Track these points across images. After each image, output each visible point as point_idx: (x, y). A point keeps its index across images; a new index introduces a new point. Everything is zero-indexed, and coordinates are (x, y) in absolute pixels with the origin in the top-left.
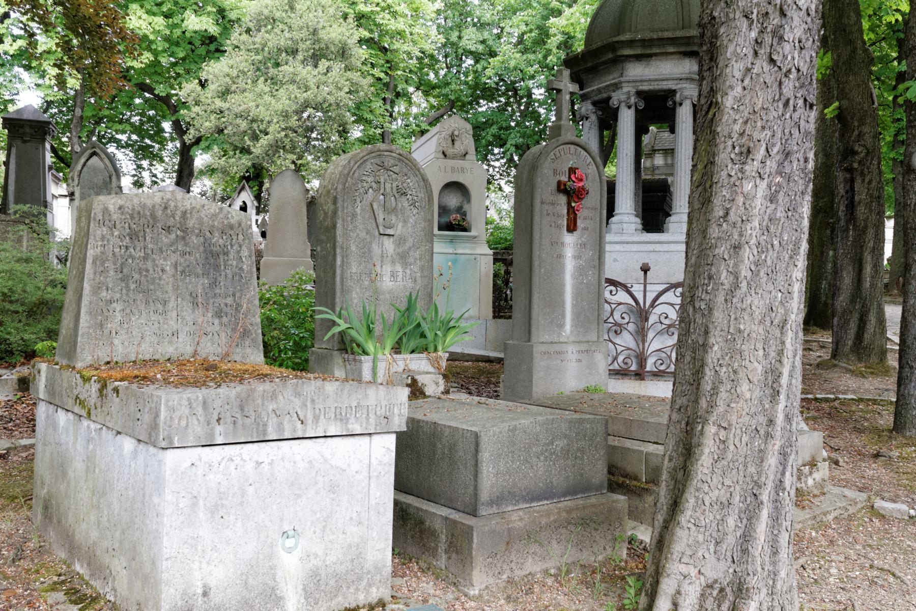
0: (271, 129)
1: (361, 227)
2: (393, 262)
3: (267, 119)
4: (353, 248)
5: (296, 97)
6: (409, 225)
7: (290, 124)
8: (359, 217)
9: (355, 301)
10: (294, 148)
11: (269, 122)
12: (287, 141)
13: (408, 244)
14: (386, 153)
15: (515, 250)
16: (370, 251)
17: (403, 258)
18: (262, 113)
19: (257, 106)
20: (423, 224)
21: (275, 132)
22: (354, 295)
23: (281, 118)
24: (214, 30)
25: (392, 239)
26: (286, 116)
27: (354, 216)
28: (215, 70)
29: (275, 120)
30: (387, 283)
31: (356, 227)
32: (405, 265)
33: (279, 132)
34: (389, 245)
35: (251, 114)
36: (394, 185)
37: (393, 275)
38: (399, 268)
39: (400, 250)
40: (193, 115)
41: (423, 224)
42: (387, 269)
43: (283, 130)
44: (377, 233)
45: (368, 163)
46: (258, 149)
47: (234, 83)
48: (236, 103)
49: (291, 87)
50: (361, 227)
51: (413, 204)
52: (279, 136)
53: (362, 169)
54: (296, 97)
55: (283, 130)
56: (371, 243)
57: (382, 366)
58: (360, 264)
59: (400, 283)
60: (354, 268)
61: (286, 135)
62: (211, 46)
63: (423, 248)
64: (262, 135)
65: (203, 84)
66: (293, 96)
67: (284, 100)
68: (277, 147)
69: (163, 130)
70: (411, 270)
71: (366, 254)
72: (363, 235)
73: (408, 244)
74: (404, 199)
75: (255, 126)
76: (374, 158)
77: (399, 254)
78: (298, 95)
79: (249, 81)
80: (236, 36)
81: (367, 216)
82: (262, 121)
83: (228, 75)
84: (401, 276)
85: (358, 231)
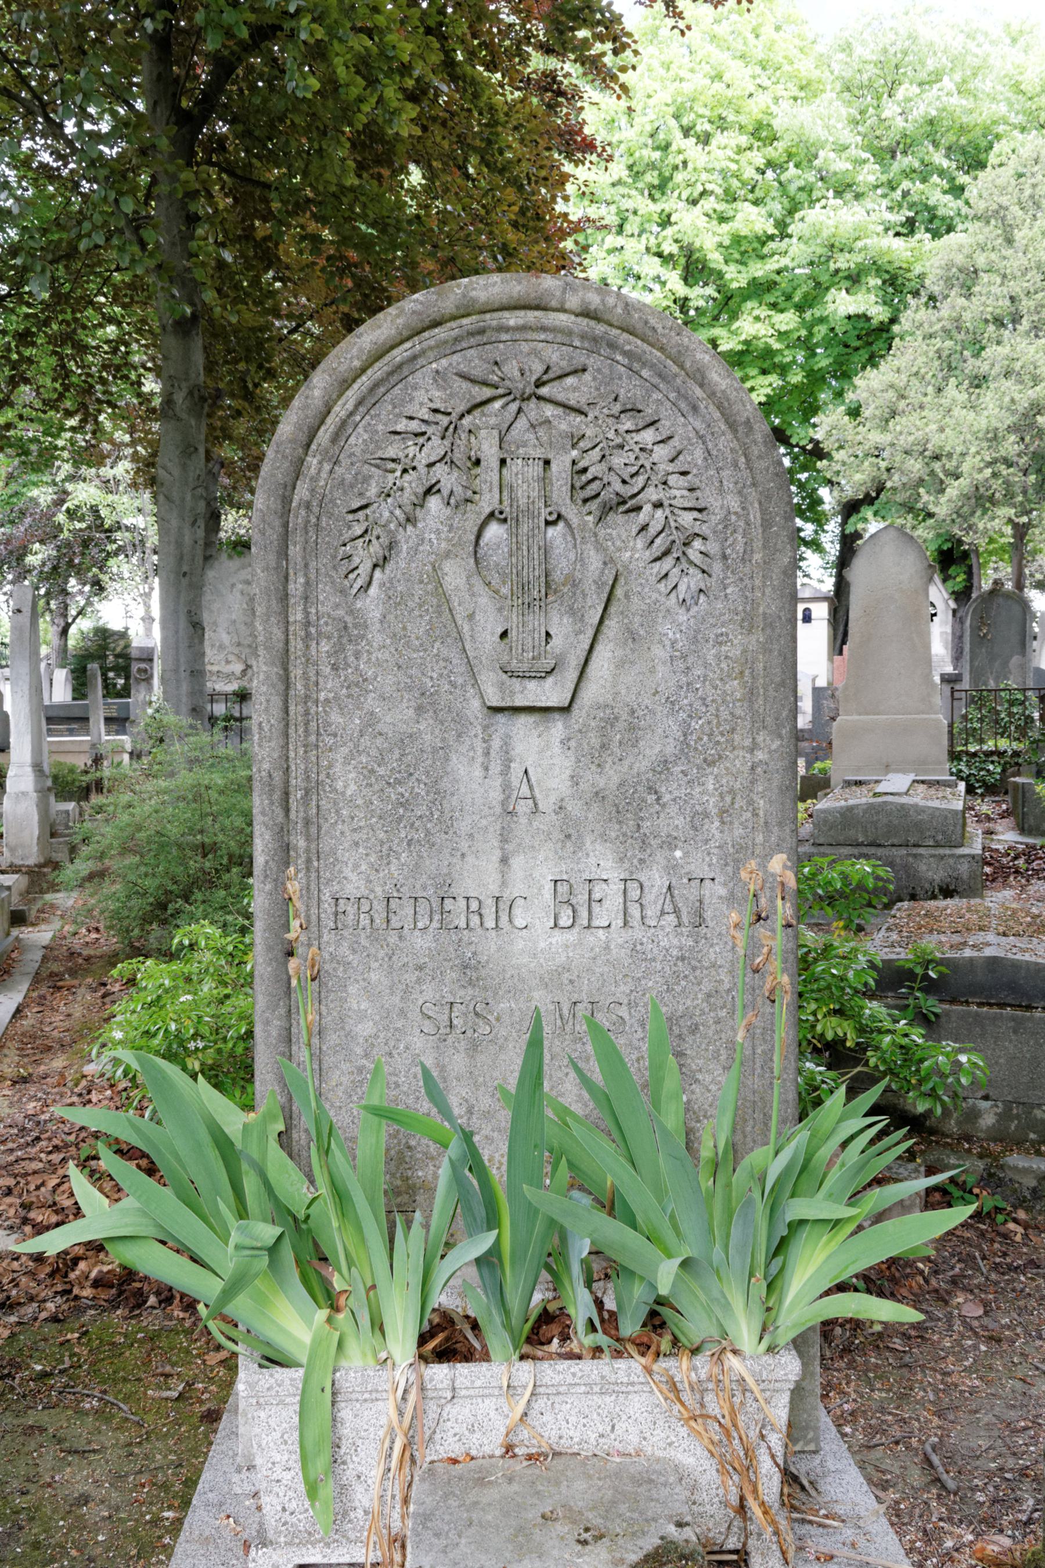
0: (965, 468)
1: (387, 682)
2: (570, 836)
3: (959, 450)
4: (347, 780)
5: (1013, 401)
6: (660, 653)
7: (1003, 453)
8: (376, 636)
9: (365, 1029)
10: (1009, 495)
11: (963, 455)
12: (997, 484)
13: (653, 747)
14: (512, 319)
15: (80, 1222)
16: (438, 794)
17: (627, 813)
18: (950, 441)
19: (942, 430)
20: (738, 643)
21: (973, 470)
22: (356, 1000)
23: (985, 444)
24: (879, 313)
25: (558, 728)
26: (994, 438)
27: (349, 632)
28: (870, 384)
29: (973, 450)
30: (536, 942)
31: (360, 685)
32: (638, 844)
33: (980, 470)
34: (544, 756)
35: (929, 446)
36: (561, 466)
37: (573, 902)
38: (602, 862)
39: (610, 778)
40: (837, 467)
41: (738, 643)
42: (536, 872)
43: (989, 464)
44: (476, 703)
45: (423, 377)
46: (942, 508)
47: (903, 397)
48: (910, 428)
49: (1008, 384)
50: (387, 682)
51: (674, 549)
52: (980, 477)
53: (385, 409)
54: (1013, 401)
55: (989, 464)
56: (442, 752)
57: (369, 1425)
58: (386, 856)
59: (610, 931)
60: (354, 874)
61: (995, 475)
62: (871, 340)
63: (739, 761)
64: (948, 481)
65: (854, 412)
66: (1007, 399)
67: (994, 408)
68: (981, 500)
69: (820, 501)
70: (672, 868)
71: (416, 808)
72: (397, 717)
73: (653, 747)
74: (621, 527)
75: (937, 466)
76: (453, 346)
77: (599, 796)
78: (1017, 396)
79: (930, 389)
80: (914, 315)
81: (418, 629)
82: (950, 455)
83: (892, 386)
84: (614, 901)
85: (371, 702)
